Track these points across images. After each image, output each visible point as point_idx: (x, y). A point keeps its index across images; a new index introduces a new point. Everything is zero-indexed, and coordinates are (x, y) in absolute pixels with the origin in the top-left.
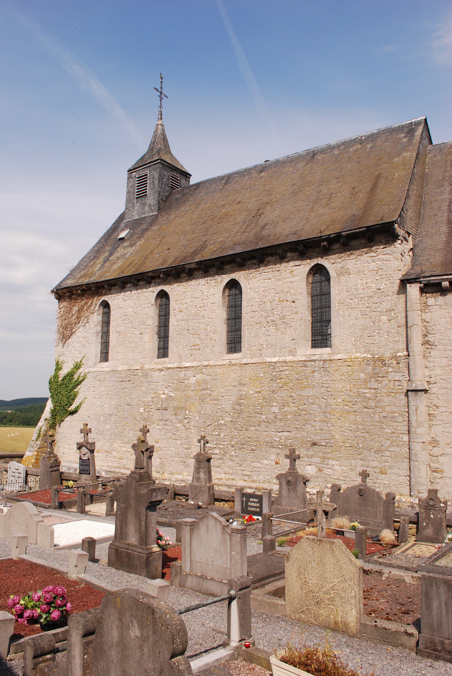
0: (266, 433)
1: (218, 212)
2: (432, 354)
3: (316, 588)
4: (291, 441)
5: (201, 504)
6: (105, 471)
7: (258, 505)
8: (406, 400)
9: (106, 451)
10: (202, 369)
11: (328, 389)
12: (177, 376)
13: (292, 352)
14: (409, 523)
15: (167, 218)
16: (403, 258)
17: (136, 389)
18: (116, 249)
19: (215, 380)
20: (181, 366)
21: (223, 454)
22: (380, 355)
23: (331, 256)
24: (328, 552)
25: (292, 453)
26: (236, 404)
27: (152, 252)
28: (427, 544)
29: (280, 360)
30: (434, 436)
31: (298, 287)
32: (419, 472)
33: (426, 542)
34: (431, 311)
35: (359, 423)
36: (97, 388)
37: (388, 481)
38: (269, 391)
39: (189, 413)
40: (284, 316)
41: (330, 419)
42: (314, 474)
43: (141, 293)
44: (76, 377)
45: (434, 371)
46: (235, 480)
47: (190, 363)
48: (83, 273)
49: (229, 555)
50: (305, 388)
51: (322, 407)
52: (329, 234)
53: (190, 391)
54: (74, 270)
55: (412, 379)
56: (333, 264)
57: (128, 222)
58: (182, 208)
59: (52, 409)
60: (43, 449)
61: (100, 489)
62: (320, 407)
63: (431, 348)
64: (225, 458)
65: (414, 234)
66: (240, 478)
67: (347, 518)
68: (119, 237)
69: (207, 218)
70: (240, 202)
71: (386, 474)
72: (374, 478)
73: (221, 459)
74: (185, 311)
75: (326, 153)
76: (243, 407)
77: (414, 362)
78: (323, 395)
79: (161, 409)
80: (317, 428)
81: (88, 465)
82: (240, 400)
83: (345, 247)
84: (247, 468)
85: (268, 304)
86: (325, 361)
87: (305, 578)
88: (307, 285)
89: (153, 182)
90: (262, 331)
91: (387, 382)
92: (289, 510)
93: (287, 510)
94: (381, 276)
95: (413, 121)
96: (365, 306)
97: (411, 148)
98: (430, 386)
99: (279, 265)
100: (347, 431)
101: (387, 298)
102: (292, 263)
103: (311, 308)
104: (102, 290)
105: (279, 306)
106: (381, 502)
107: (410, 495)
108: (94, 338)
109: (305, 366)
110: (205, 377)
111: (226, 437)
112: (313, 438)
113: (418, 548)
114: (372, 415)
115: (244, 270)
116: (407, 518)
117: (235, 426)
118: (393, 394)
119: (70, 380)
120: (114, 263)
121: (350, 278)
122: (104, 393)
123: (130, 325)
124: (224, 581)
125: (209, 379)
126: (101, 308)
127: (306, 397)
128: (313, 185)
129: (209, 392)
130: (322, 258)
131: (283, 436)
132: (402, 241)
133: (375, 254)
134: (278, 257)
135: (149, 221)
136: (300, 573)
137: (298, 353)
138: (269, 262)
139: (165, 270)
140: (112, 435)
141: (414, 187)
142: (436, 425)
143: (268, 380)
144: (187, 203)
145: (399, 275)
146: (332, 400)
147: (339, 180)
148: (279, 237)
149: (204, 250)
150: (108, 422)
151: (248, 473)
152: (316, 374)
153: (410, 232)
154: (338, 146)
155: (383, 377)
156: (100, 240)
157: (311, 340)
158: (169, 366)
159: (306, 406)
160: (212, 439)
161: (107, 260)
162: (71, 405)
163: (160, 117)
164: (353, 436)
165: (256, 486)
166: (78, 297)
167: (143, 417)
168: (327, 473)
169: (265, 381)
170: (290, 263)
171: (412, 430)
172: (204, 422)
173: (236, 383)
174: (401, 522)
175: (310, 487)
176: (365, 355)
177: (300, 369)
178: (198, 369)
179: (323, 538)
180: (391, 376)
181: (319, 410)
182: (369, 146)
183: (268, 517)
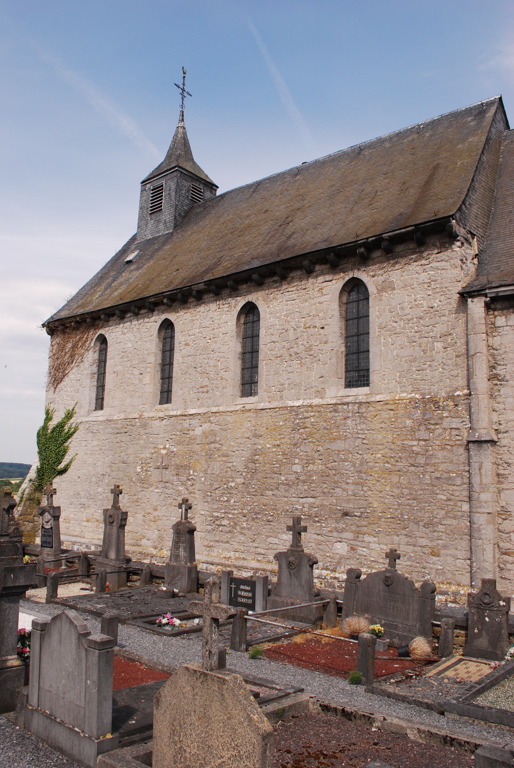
0: (286, 499)
1: (241, 224)
2: (502, 392)
3: (196, 763)
4: (317, 509)
5: (177, 591)
6: (95, 545)
7: (250, 595)
8: (466, 454)
9: (97, 521)
10: (210, 417)
11: (365, 441)
12: (181, 425)
13: (321, 393)
14: (455, 628)
15: (182, 235)
16: (464, 266)
17: (133, 442)
18: (121, 274)
19: (225, 430)
20: (186, 413)
21: (232, 526)
22: (432, 394)
23: (371, 267)
24: (216, 699)
25: (296, 523)
26: (250, 461)
27: (159, 275)
28: (479, 660)
29: (304, 404)
30: (504, 504)
31: (328, 309)
32: (483, 553)
33: (477, 658)
34: (500, 334)
35: (404, 486)
36: (89, 442)
37: (441, 566)
38: (290, 444)
39: (193, 472)
40: (311, 346)
41: (366, 482)
42: (345, 554)
43: (142, 324)
44: (66, 428)
45: (504, 416)
46: (246, 559)
47: (196, 410)
48: (80, 303)
49: (84, 684)
50: (334, 439)
51: (357, 465)
52: (366, 237)
53: (195, 445)
54: (71, 300)
55: (475, 426)
56: (373, 276)
57: (139, 243)
58: (201, 223)
59: (39, 467)
60: (26, 516)
61: (64, 567)
62: (354, 465)
63: (501, 384)
64: (235, 531)
65: (480, 237)
66: (253, 557)
67: (366, 618)
68: (126, 261)
69: (227, 231)
70: (267, 211)
71: (439, 556)
72: (423, 561)
73: (230, 532)
74: (192, 344)
75: (373, 148)
76: (258, 465)
77: (477, 403)
78: (357, 448)
79: (161, 467)
80: (350, 493)
81: (51, 536)
82: (255, 456)
83: (388, 254)
84: (261, 545)
85: (291, 332)
86: (360, 403)
87: (180, 742)
88: (340, 306)
89: (169, 193)
90: (283, 367)
91: (440, 431)
92: (289, 604)
93: (287, 603)
94: (435, 290)
95: (484, 101)
96: (413, 330)
97: (479, 132)
98: (500, 436)
99: (306, 282)
100: (388, 497)
101: (443, 318)
102: (321, 279)
103: (344, 335)
104: (98, 322)
105: (304, 334)
106: (415, 596)
107: (471, 585)
108: (88, 381)
109: (336, 411)
110: (213, 427)
111: (236, 504)
112: (344, 505)
113: (465, 666)
114: (421, 476)
115: (263, 290)
116: (451, 621)
117: (248, 490)
118: (449, 447)
119: (60, 432)
120: (116, 290)
121: (394, 295)
122: (97, 449)
123: (129, 364)
124: (76, 729)
125: (217, 429)
126: (98, 344)
127: (336, 452)
128: (355, 184)
129: (217, 446)
130: (359, 269)
131: (306, 503)
132: (462, 244)
133: (426, 262)
134: (304, 271)
135: (163, 240)
136: (174, 731)
137: (327, 395)
138: (293, 278)
139: (169, 293)
140: (104, 500)
141: (482, 178)
142: (507, 489)
143: (290, 430)
144: (207, 217)
145: (459, 287)
146: (369, 455)
147: (388, 175)
148: (306, 246)
149: (217, 267)
150: (101, 484)
151: (263, 552)
152: (349, 422)
153: (475, 233)
154: (390, 138)
155: (436, 424)
156: (106, 265)
157: (344, 377)
158: (172, 413)
159: (336, 464)
160: (220, 506)
161: (109, 285)
162: (60, 463)
163: (181, 119)
164: (396, 503)
165: (271, 569)
166: (73, 331)
167: (140, 477)
168: (362, 553)
169: (285, 431)
170: (319, 278)
171: (475, 495)
172: (210, 484)
173: (249, 434)
174: (442, 626)
175: (340, 571)
176: (413, 395)
177: (329, 414)
178: (205, 417)
179: (211, 670)
180: (446, 423)
181: (352, 469)
182: (427, 135)
183: (240, 615)
